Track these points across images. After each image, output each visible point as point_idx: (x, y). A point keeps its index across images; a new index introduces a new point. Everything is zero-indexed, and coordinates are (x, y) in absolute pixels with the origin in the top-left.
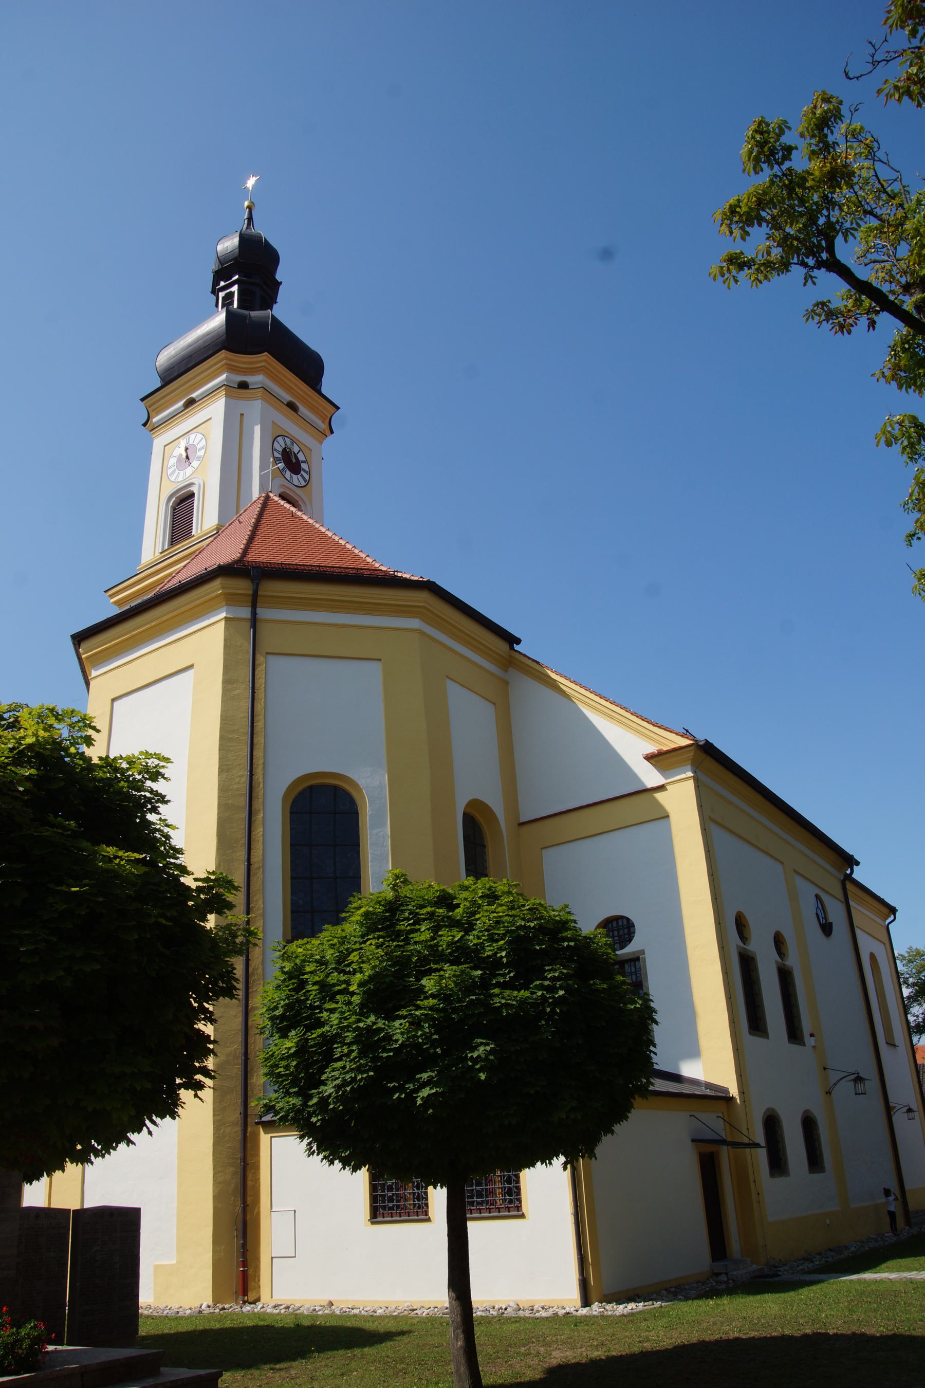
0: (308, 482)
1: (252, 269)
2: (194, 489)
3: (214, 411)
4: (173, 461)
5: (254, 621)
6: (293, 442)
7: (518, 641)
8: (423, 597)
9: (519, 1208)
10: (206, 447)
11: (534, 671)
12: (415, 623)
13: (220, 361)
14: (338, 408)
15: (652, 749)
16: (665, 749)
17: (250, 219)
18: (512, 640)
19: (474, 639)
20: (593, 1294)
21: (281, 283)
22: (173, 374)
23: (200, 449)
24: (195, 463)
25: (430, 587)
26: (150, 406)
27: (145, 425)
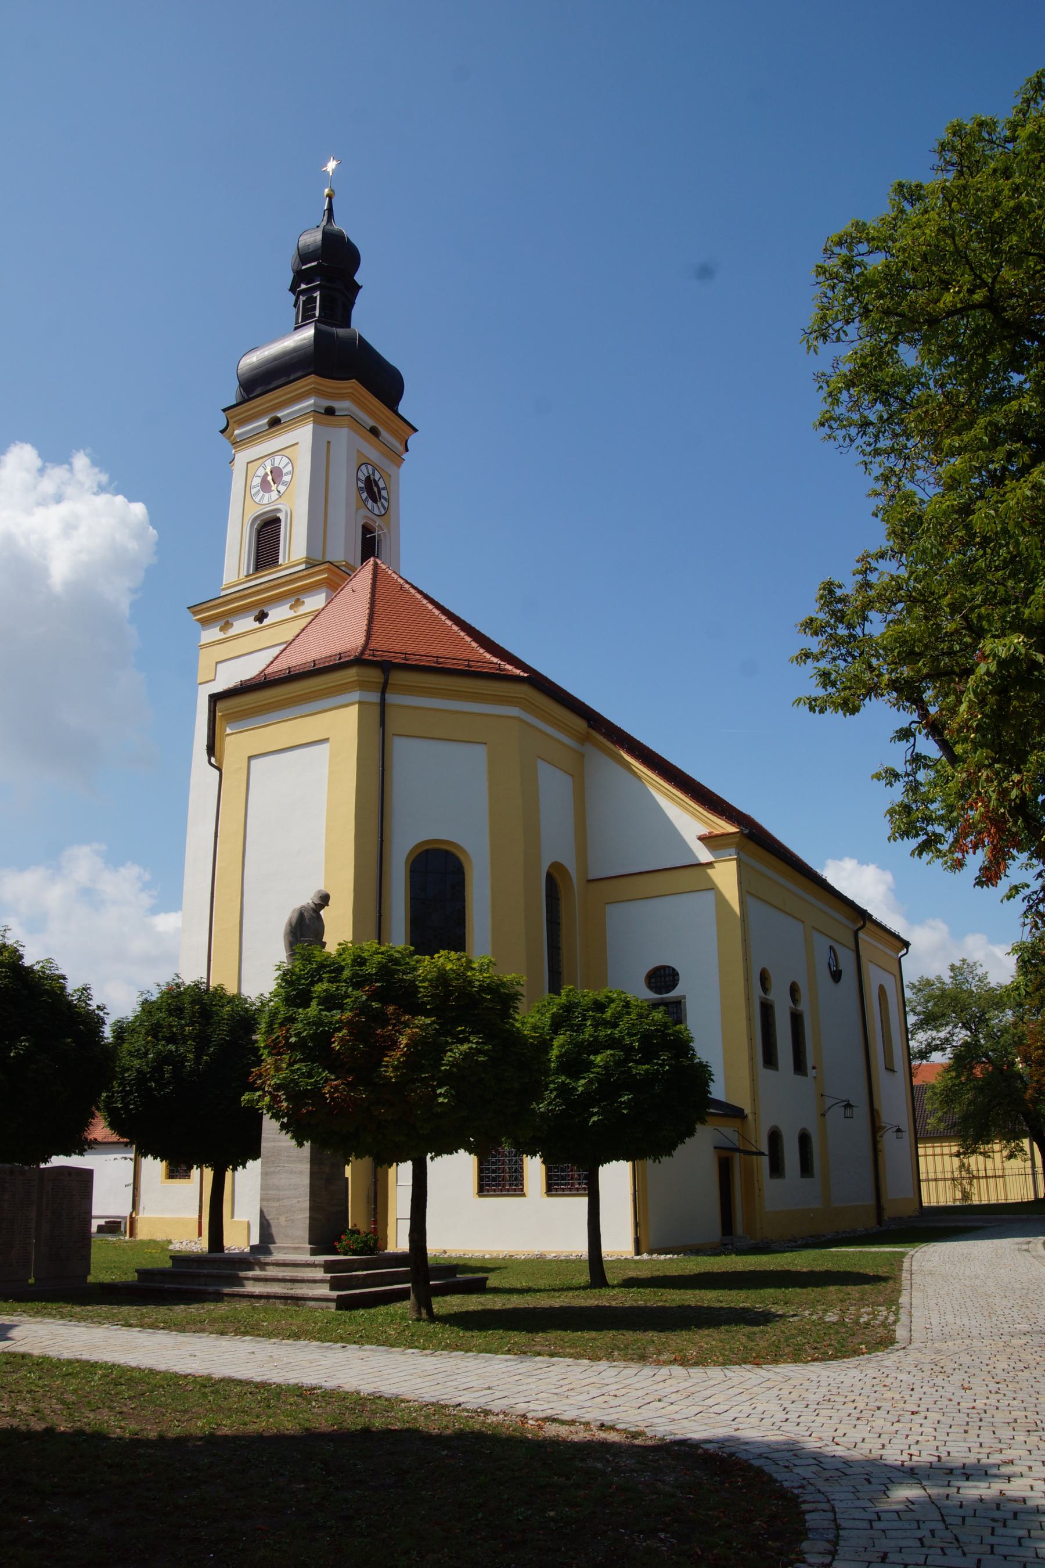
0: (387, 510)
1: (329, 274)
2: (281, 516)
3: (303, 435)
5: (383, 704)
9: (522, 1190)
10: (292, 473)
12: (514, 711)
13: (309, 384)
14: (416, 430)
15: (704, 831)
16: (716, 832)
17: (330, 210)
21: (361, 287)
23: (286, 474)
27: (222, 432)
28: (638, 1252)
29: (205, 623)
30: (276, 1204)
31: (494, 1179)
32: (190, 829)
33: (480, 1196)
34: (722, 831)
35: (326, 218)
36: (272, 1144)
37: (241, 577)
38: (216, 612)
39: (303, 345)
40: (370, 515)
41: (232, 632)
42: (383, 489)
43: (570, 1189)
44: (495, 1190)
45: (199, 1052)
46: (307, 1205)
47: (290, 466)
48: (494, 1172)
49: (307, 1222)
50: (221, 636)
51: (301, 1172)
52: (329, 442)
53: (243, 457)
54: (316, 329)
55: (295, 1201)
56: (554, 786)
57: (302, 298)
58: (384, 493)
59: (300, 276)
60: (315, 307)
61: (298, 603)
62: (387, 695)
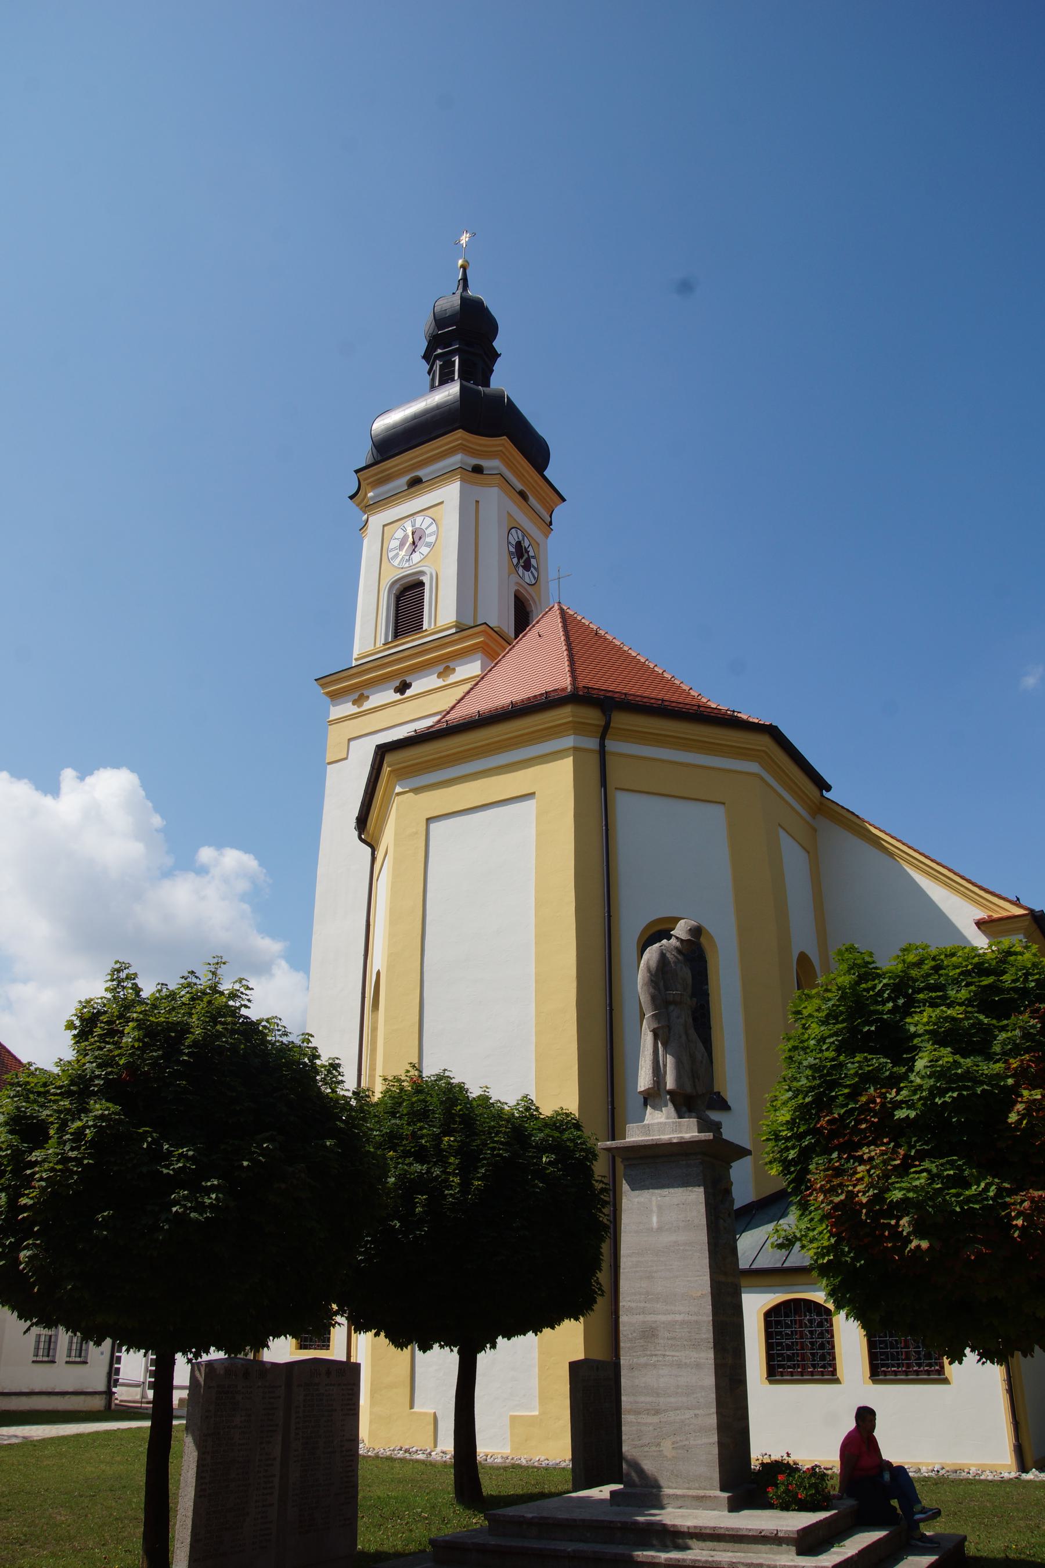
0: (537, 579)
1: (464, 338)
2: (425, 579)
3: (450, 493)
4: (394, 544)
5: (602, 752)
6: (523, 536)
7: (828, 788)
8: (765, 742)
9: (834, 1372)
10: (437, 533)
11: (851, 823)
12: (754, 767)
13: (457, 440)
14: (564, 500)
15: (981, 914)
16: (995, 916)
17: (465, 279)
18: (823, 785)
19: (795, 783)
20: (1029, 1460)
21: (499, 355)
22: (391, 446)
23: (430, 535)
24: (424, 550)
25: (773, 732)
26: (365, 480)
27: (351, 497)
28: (1023, 1468)
29: (335, 696)
30: (655, 1419)
31: (790, 1358)
32: (316, 927)
33: (771, 1382)
34: (1005, 914)
35: (461, 286)
36: (641, 1318)
37: (378, 645)
38: (348, 684)
39: (447, 402)
40: (521, 581)
41: (367, 705)
42: (533, 557)
43: (906, 1373)
44: (792, 1374)
45: (466, 1171)
46: (713, 1420)
47: (434, 528)
48: (789, 1347)
49: (715, 1450)
50: (355, 709)
51: (698, 1366)
52: (477, 502)
53: (377, 520)
54: (463, 388)
55: (689, 1414)
56: (794, 859)
57: (438, 363)
58: (533, 562)
59: (435, 341)
60: (454, 371)
61: (447, 671)
62: (606, 741)
